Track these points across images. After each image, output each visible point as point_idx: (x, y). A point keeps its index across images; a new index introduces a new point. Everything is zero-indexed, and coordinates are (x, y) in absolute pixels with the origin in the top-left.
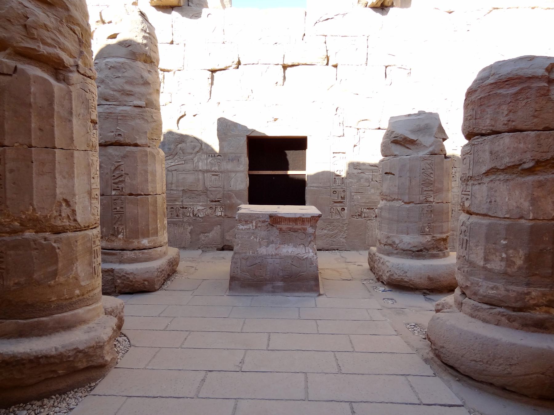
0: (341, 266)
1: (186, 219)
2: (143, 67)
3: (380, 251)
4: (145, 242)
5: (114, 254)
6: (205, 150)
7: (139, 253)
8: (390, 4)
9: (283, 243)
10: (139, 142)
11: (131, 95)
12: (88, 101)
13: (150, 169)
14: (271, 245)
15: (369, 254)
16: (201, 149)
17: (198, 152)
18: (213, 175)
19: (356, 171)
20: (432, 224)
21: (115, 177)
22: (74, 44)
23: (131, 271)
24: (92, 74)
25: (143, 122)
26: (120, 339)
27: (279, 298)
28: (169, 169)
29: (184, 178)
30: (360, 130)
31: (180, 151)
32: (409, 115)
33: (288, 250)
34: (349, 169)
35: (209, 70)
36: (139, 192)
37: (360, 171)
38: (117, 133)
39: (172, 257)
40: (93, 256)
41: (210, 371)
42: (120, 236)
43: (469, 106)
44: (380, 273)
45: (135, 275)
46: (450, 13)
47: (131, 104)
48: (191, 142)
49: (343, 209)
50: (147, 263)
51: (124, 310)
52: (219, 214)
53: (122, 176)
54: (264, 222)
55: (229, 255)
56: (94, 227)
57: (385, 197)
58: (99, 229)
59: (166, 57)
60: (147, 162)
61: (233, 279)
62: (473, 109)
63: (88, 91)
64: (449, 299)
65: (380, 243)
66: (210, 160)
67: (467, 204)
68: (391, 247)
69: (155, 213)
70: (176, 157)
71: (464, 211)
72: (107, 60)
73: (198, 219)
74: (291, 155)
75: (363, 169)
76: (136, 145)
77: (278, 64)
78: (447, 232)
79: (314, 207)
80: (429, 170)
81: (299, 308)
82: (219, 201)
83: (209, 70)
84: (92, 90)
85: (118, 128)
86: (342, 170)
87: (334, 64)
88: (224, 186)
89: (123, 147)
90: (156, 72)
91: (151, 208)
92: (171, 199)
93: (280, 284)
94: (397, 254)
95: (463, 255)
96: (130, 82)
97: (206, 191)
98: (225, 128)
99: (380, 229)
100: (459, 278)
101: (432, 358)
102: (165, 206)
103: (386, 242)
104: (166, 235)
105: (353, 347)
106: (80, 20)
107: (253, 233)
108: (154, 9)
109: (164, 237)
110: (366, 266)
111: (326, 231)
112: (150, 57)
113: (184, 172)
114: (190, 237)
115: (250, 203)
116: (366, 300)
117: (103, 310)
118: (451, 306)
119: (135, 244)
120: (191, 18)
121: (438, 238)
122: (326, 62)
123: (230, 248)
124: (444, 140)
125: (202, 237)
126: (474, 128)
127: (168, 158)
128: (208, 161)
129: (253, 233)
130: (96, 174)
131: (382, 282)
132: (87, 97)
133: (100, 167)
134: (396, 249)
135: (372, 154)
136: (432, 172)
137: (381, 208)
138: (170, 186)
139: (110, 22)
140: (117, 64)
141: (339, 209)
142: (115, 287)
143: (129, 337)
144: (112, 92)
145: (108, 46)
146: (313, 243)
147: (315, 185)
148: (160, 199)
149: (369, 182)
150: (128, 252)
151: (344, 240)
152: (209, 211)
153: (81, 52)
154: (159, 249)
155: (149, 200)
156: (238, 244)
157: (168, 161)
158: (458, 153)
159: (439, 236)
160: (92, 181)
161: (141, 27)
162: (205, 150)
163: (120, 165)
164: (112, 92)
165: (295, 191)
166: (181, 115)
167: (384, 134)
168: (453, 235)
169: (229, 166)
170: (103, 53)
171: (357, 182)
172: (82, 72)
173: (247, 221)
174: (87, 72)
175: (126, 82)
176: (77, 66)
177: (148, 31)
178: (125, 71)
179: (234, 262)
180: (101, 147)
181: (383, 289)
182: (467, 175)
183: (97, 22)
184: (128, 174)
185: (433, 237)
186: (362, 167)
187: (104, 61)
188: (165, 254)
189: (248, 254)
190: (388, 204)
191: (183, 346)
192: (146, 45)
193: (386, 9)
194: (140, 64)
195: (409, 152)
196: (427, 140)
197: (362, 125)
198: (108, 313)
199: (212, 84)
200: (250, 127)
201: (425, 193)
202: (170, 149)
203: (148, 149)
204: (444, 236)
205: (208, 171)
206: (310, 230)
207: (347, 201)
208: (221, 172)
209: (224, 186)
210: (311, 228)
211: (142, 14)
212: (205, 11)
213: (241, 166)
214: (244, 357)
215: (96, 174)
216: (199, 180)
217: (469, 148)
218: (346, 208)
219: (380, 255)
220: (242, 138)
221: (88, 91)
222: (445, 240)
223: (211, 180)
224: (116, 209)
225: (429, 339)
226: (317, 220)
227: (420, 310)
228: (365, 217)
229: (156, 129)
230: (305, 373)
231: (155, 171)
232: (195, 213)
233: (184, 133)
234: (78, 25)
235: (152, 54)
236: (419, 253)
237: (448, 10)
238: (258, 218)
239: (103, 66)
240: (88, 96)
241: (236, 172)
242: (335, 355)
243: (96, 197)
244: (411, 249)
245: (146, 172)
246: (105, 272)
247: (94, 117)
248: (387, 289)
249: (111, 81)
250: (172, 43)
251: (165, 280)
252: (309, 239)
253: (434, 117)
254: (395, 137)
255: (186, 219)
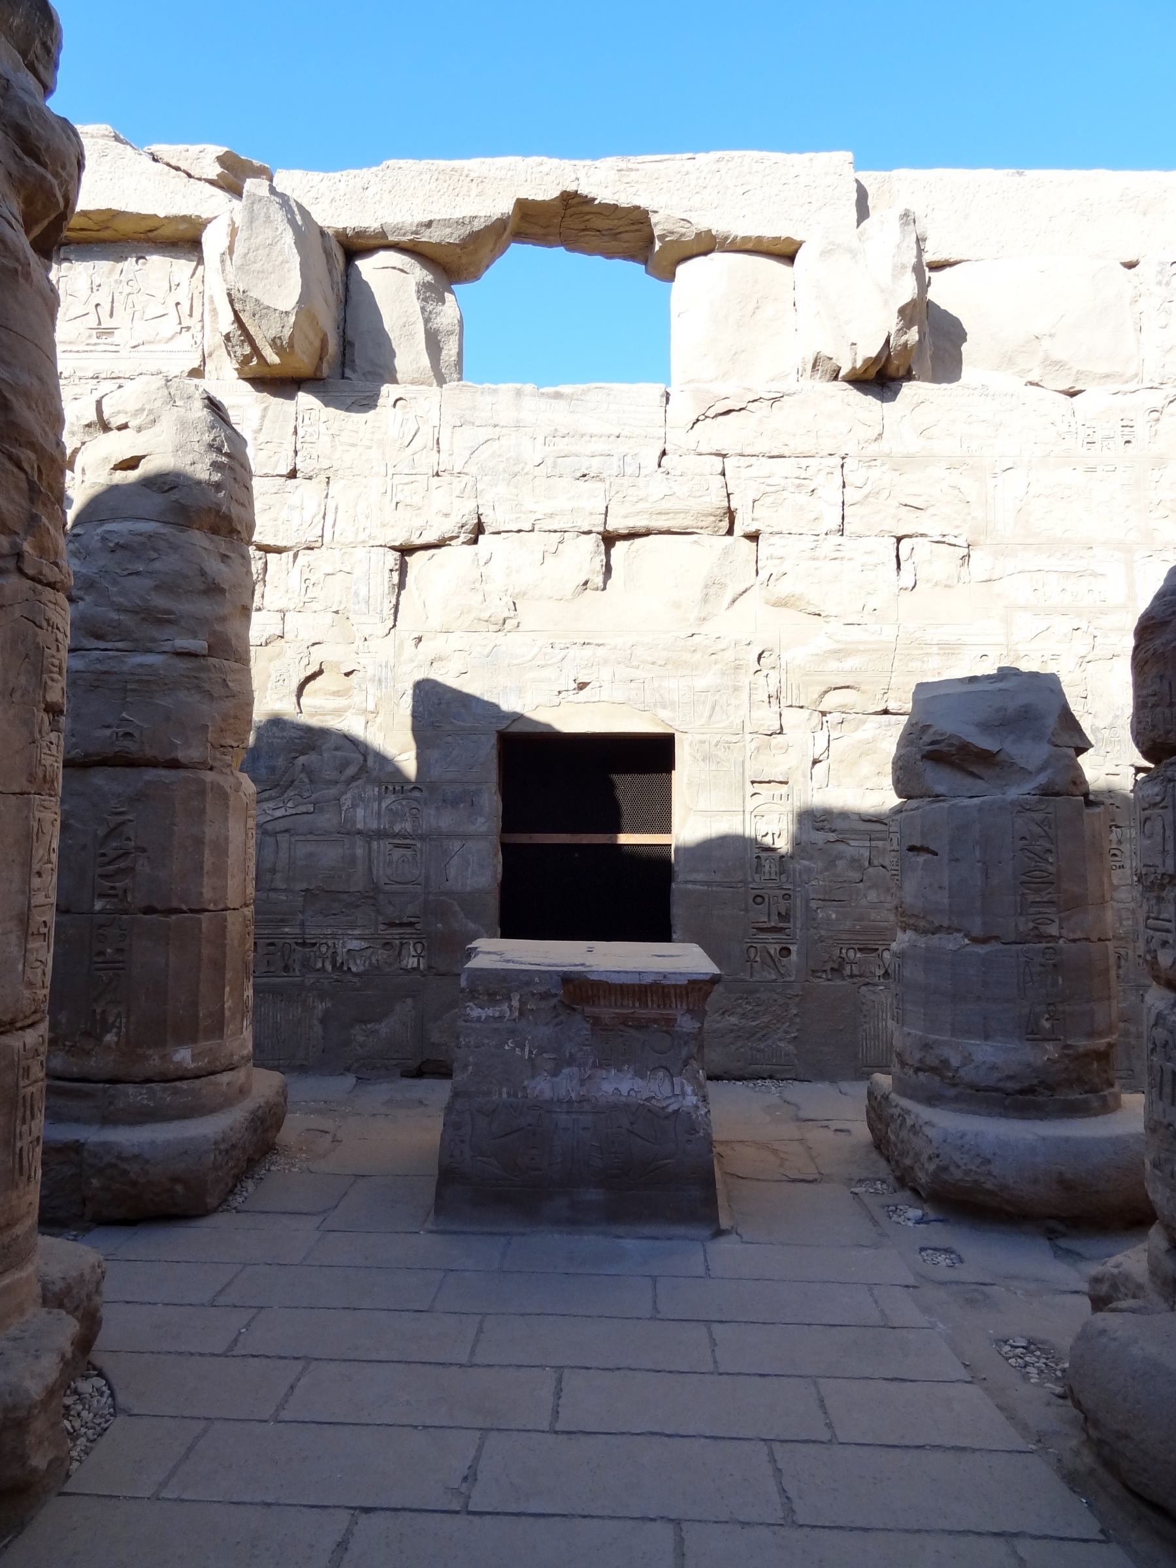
0: (782, 1130)
1: (310, 979)
2: (206, 543)
3: (903, 1088)
4: (184, 1056)
5: (88, 1095)
6: (375, 774)
7: (165, 1090)
8: (902, 372)
9: (604, 1063)
10: (181, 755)
11: (169, 621)
12: (40, 650)
13: (210, 832)
14: (566, 1071)
15: (871, 1094)
16: (363, 769)
17: (354, 778)
18: (397, 846)
19: (819, 837)
20: (1060, 1008)
21: (106, 859)
22: (16, 497)
23: (136, 1151)
24: (59, 577)
25: (198, 697)
26: (85, 1387)
27: (590, 1242)
28: (269, 827)
29: (311, 855)
30: (829, 717)
31: (303, 776)
32: (973, 680)
33: (619, 1085)
34: (800, 829)
35: (394, 548)
36: (175, 904)
37: (832, 837)
38: (122, 730)
39: (262, 1101)
40: (20, 1115)
41: (367, 1510)
42: (110, 1038)
43: (1146, 668)
44: (908, 1162)
45: (147, 1161)
46: (1073, 394)
47: (167, 646)
48: (336, 749)
49: (786, 951)
50: (187, 1123)
51: (105, 1286)
52: (412, 962)
53: (127, 854)
54: (544, 996)
55: (438, 1091)
56: (29, 1021)
57: (912, 921)
58: (43, 1028)
59: (273, 514)
60: (203, 812)
61: (448, 1176)
62: (1161, 677)
63: (45, 624)
64: (1134, 1258)
65: (903, 1064)
66: (388, 801)
67: (1165, 959)
68: (937, 1079)
69: (219, 966)
70: (291, 793)
71: (1156, 978)
72: (108, 527)
73: (349, 977)
74: (627, 786)
75: (843, 831)
76: (174, 764)
77: (589, 532)
78: (1110, 1031)
79: (695, 949)
80: (1041, 842)
81: (655, 1279)
82: (411, 924)
83: (394, 548)
84: (56, 619)
85: (124, 715)
86: (775, 828)
87: (752, 529)
88: (427, 879)
89: (135, 770)
90: (246, 560)
91: (207, 951)
92: (268, 916)
93: (594, 1195)
94: (956, 1099)
95: (1165, 1121)
96: (167, 586)
97: (373, 894)
98: (436, 708)
99: (900, 1020)
100: (1158, 1194)
101: (1091, 1472)
102: (250, 944)
103: (921, 1060)
104: (248, 1034)
105: (829, 1425)
106: (38, 431)
107: (513, 1032)
108: (247, 386)
109: (241, 1039)
110: (862, 1132)
111: (733, 1020)
112: (227, 518)
113: (310, 837)
114: (321, 1032)
115: (508, 932)
116: (866, 1252)
117: (37, 1289)
118: (1140, 1287)
119: (154, 1062)
120: (348, 410)
121: (1081, 1050)
122: (725, 524)
123: (442, 1071)
124: (1081, 750)
125: (358, 1034)
126: (1168, 732)
127: (266, 795)
128: (384, 805)
129: (513, 1032)
130: (49, 862)
131: (915, 1191)
132: (39, 639)
133: (65, 827)
134: (954, 1085)
135: (866, 784)
136: (1048, 846)
137: (901, 955)
138: (268, 876)
139: (124, 427)
140: (138, 539)
141: (773, 949)
142: (84, 1201)
143: (113, 1381)
144: (114, 615)
145: (113, 489)
146: (694, 1064)
147: (700, 877)
148: (234, 924)
149: (862, 869)
150: (131, 1089)
151: (791, 1048)
152: (382, 955)
153: (34, 519)
154: (225, 1078)
155: (204, 926)
156: (465, 1067)
157: (265, 805)
158: (1125, 782)
159: (1082, 1044)
160: (36, 882)
161: (207, 438)
162: (375, 774)
163: (123, 823)
164: (114, 615)
165: (640, 896)
166: (309, 673)
167: (901, 728)
168: (1126, 1034)
169: (446, 821)
170: (97, 508)
171: (827, 869)
172: (31, 572)
173: (495, 994)
174: (46, 570)
175: (156, 588)
176: (19, 556)
177: (226, 449)
178: (155, 555)
179: (452, 1125)
180: (70, 770)
181: (919, 1213)
182: (1160, 870)
183: (89, 426)
184: (144, 850)
185: (1067, 1047)
186: (839, 824)
187: (99, 530)
188: (243, 1092)
189: (495, 1098)
190: (922, 941)
191: (285, 1415)
192: (218, 486)
193: (891, 384)
194: (198, 538)
195: (980, 785)
196: (1030, 753)
197: (832, 700)
198: (54, 1298)
199: (401, 585)
200: (508, 705)
201: (1032, 910)
202: (272, 769)
203: (209, 776)
204: (1101, 1043)
205: (380, 835)
206: (686, 1024)
207: (797, 924)
208: (422, 838)
209: (427, 879)
210: (688, 1016)
211: (214, 405)
212: (388, 392)
213: (481, 820)
214: (477, 1459)
215: (49, 862)
216: (353, 860)
217: (1156, 789)
218: (793, 948)
219: (905, 1103)
220: (484, 738)
221: (45, 624)
222: (1103, 1056)
223: (390, 862)
224: (101, 953)
225: (1078, 1404)
226: (708, 994)
227: (1041, 1294)
228: (852, 976)
229: (235, 717)
230: (677, 1522)
231: (226, 839)
232: (339, 960)
233: (315, 722)
234: (33, 446)
235: (235, 510)
236: (1023, 1097)
237: (1065, 387)
238: (527, 984)
239: (95, 543)
240: (43, 636)
241: (466, 837)
242: (771, 1453)
243: (43, 930)
244: (1001, 1084)
245: (199, 842)
246: (55, 1152)
247: (55, 695)
248: (932, 1215)
249: (115, 583)
250: (293, 474)
251: (238, 1179)
252: (684, 1052)
253: (1048, 685)
254: (933, 743)
255: (310, 979)
